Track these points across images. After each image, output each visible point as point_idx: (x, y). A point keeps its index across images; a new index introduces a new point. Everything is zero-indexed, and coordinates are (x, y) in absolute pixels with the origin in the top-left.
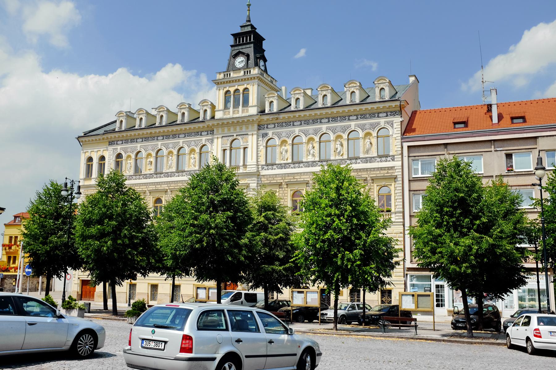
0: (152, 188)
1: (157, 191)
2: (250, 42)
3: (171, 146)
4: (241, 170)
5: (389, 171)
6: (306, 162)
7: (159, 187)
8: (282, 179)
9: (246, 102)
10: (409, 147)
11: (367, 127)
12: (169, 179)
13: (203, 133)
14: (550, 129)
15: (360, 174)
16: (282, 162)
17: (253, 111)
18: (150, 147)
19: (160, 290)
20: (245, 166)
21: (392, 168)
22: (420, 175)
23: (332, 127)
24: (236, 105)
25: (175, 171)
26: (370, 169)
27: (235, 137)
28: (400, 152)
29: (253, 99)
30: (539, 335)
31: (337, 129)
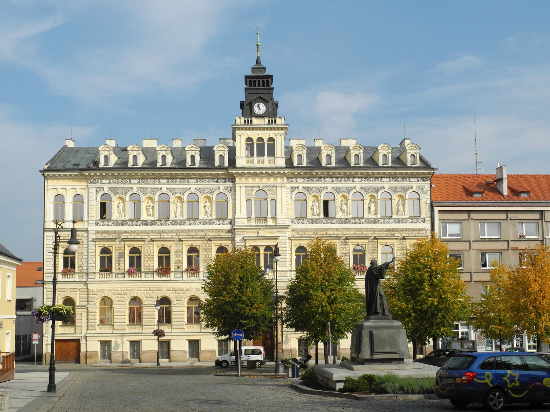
0: (153, 236)
1: (359, 238)
2: (259, 85)
3: (149, 191)
4: (270, 222)
5: (420, 232)
6: (339, 219)
7: (164, 235)
8: (314, 234)
9: (272, 153)
10: (440, 212)
11: (399, 189)
12: (178, 227)
13: (219, 180)
14: (485, 204)
15: (393, 233)
16: (314, 217)
17: (281, 162)
18: (149, 191)
19: (203, 346)
20: (274, 218)
21: (422, 229)
22: (486, 237)
23: (143, 188)
24: (261, 154)
25: (156, 219)
26: (403, 230)
27: (261, 188)
28: (429, 215)
29: (280, 150)
30: (397, 356)
31: (370, 189)
